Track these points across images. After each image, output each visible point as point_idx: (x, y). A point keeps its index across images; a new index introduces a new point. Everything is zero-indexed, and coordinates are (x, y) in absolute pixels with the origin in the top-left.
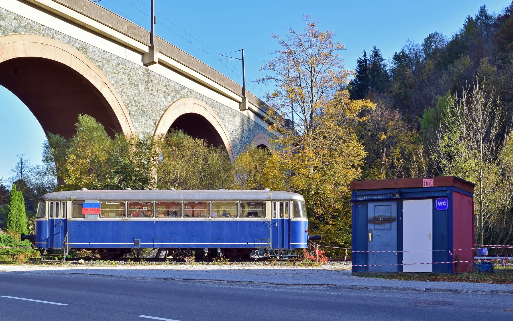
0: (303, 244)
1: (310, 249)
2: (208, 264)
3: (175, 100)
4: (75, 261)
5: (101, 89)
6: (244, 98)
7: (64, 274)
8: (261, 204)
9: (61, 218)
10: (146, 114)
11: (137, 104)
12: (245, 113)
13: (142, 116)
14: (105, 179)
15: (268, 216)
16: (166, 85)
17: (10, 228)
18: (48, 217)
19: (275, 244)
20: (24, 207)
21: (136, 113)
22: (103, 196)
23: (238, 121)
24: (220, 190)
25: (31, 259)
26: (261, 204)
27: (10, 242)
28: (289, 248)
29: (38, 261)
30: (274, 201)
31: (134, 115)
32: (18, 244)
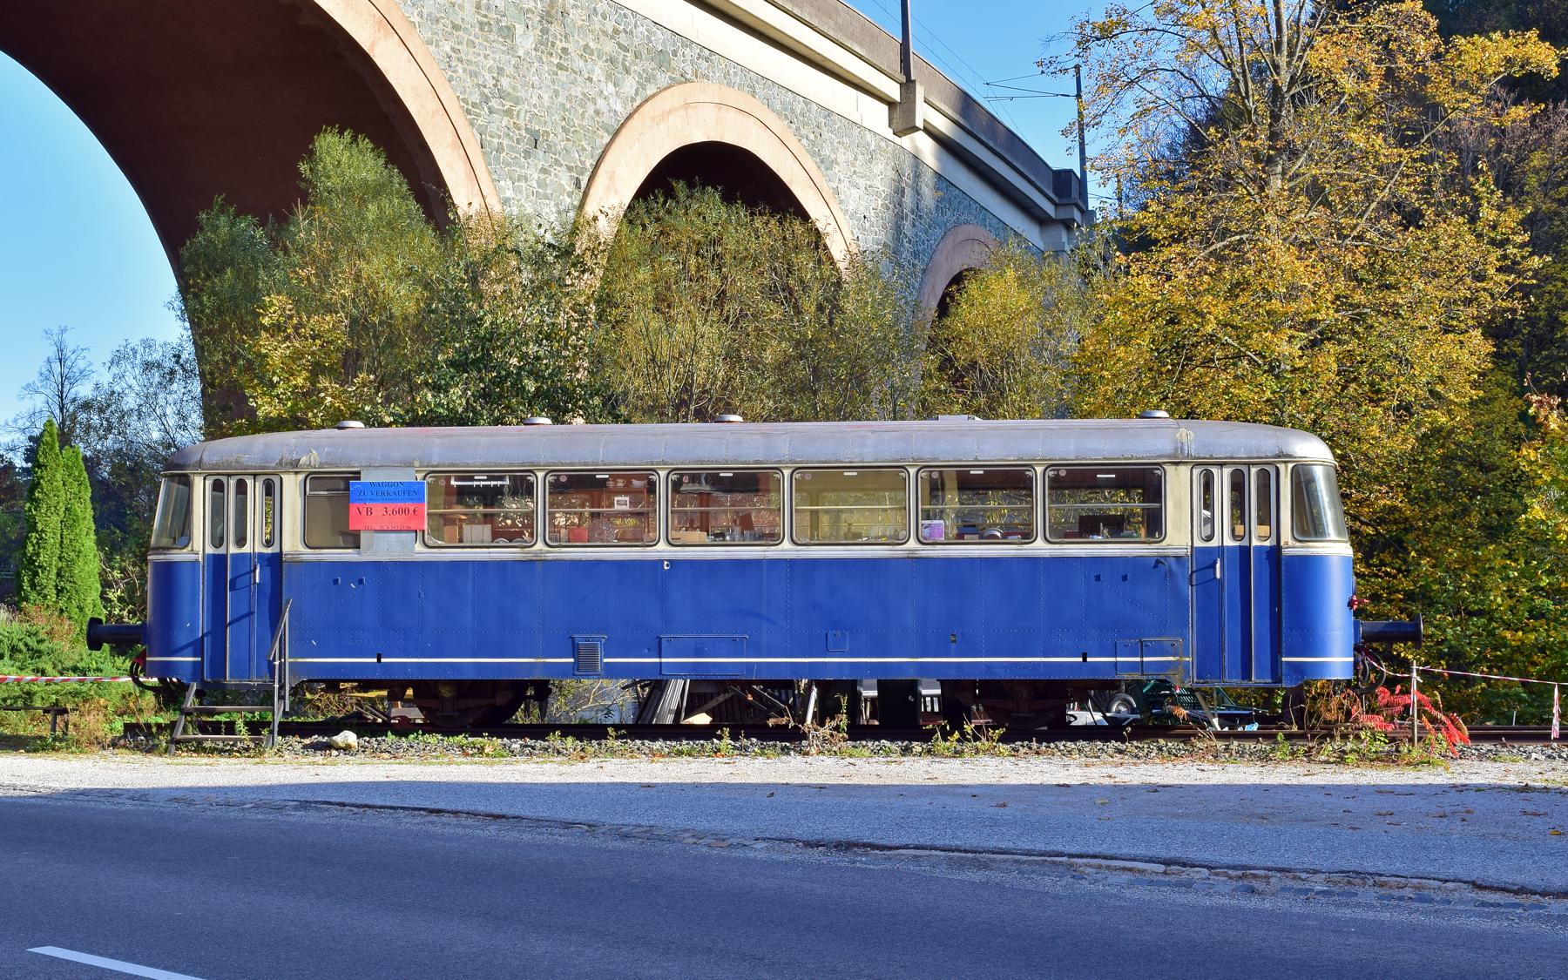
0: (1337, 661)
1: (1360, 686)
2: (906, 751)
3: (649, 93)
4: (315, 738)
5: (373, 45)
6: (908, 86)
7: (304, 805)
8: (1143, 482)
9: (260, 549)
10: (542, 145)
11: (508, 105)
12: (905, 142)
13: (527, 154)
14: (414, 388)
15: (1179, 535)
16: (616, 31)
17: (33, 596)
18: (200, 544)
19: (1209, 662)
20: (90, 513)
21: (506, 142)
22: (436, 451)
23: (881, 176)
24: (945, 421)
25: (130, 729)
26: (1143, 482)
27: (37, 654)
28: (1277, 678)
29: (163, 739)
30: (1206, 468)
31: (500, 149)
32: (69, 664)
